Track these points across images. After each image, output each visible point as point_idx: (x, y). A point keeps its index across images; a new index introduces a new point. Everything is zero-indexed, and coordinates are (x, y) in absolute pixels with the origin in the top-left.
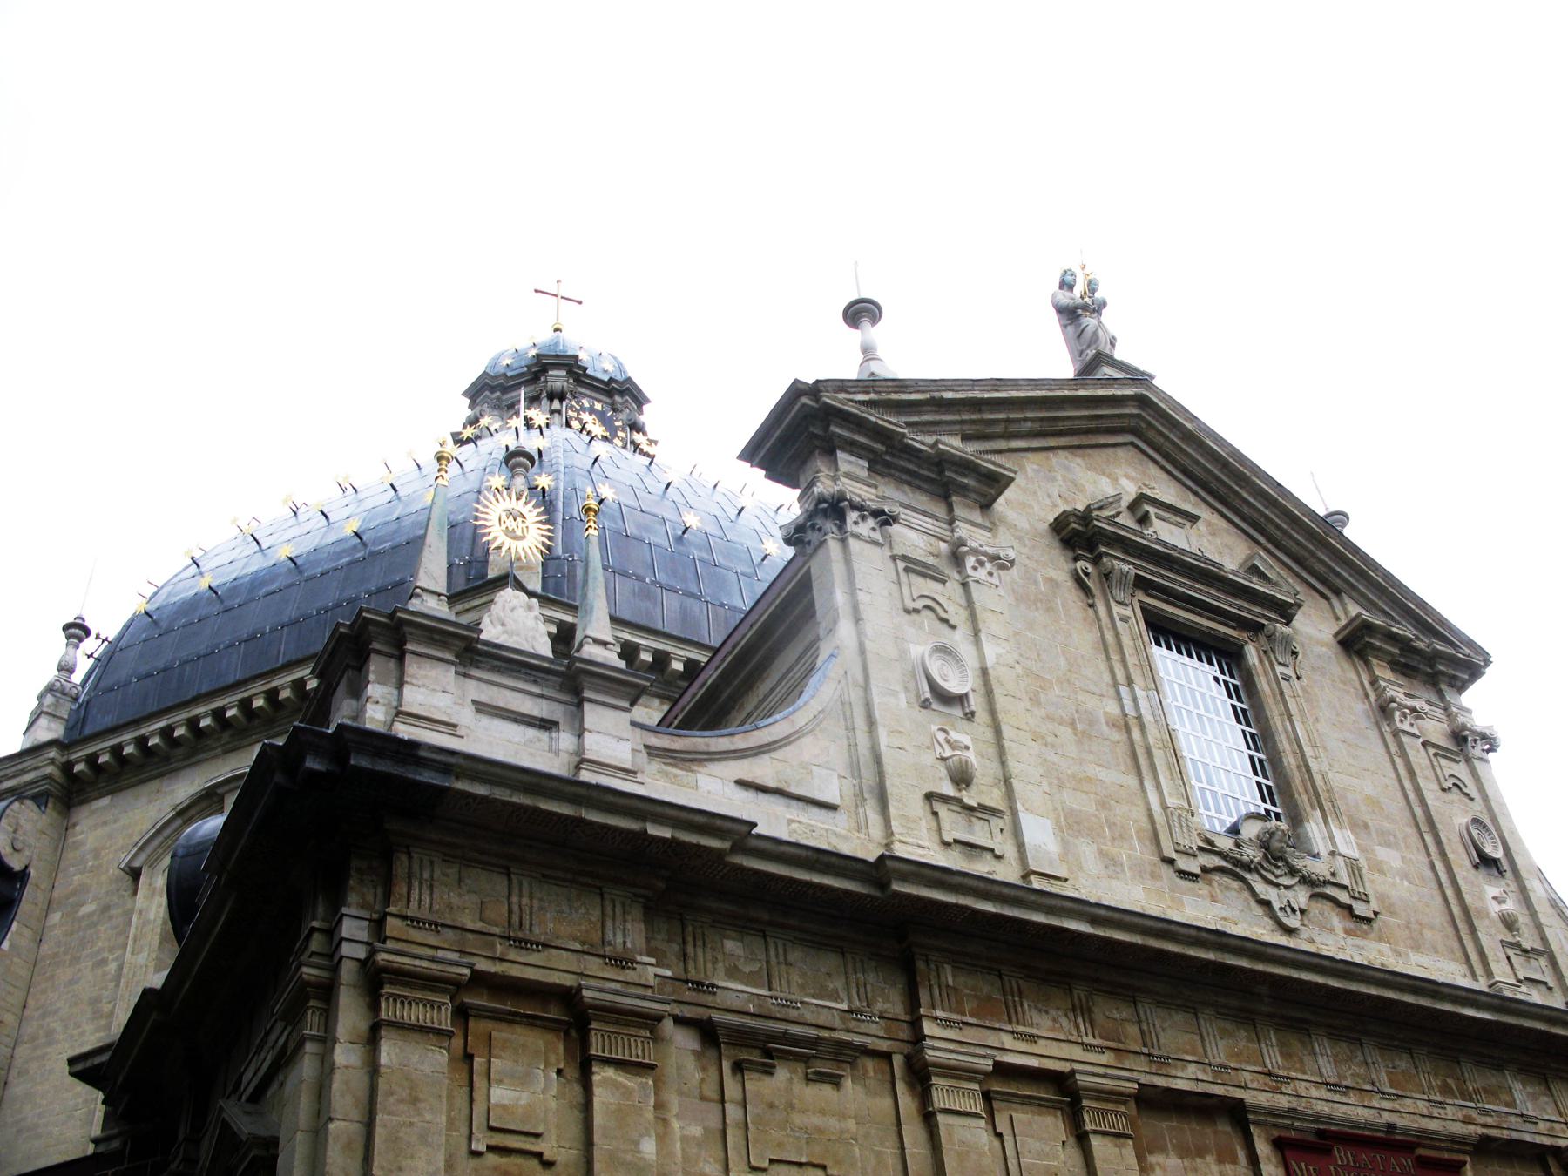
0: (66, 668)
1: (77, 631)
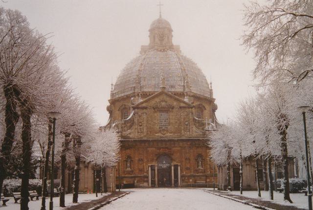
0: (112, 89)
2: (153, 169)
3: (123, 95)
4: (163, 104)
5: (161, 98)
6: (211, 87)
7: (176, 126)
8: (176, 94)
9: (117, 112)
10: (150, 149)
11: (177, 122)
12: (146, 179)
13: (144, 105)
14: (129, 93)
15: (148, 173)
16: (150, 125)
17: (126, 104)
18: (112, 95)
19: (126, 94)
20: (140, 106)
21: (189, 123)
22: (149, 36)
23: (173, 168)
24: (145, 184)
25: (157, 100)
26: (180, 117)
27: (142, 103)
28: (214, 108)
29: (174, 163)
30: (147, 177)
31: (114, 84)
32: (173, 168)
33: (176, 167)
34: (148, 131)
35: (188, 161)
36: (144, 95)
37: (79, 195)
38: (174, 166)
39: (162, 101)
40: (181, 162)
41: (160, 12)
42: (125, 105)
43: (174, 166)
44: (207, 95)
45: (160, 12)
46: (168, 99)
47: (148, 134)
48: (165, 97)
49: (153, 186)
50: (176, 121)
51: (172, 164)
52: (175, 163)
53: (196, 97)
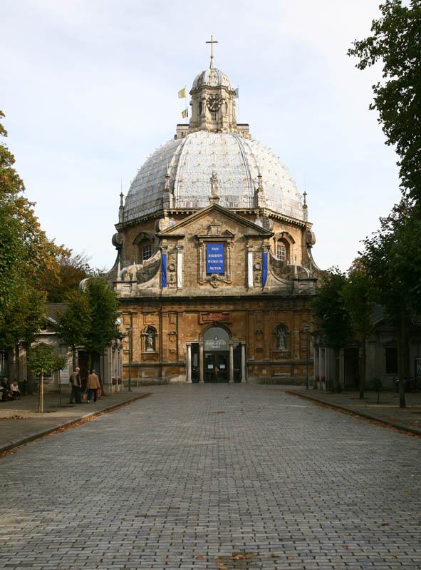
1: (122, 195)
45: (212, 58)
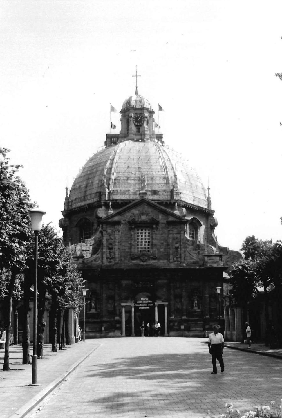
0: (67, 194)
1: (67, 189)
2: (128, 312)
3: (82, 204)
4: (144, 218)
5: (140, 208)
6: (209, 194)
7: (161, 250)
8: (160, 202)
9: (74, 229)
10: (124, 283)
11: (162, 244)
12: (118, 325)
13: (116, 219)
14: (92, 201)
15: (121, 316)
16: (123, 248)
17: (88, 217)
18: (68, 202)
19: (88, 202)
20: (110, 220)
21: (181, 245)
22: (121, 120)
23: (156, 309)
24: (118, 333)
25: (136, 212)
26: (168, 237)
27: (113, 216)
28: (212, 226)
29: (158, 303)
30: (120, 322)
31: (70, 188)
32: (156, 309)
33: (161, 308)
34: (121, 256)
35: (178, 300)
36: (116, 204)
37: (4, 357)
38: (159, 306)
39: (143, 214)
40: (168, 300)
41: (137, 87)
42: (86, 219)
43: (159, 306)
44: (204, 205)
45: (137, 87)
46: (150, 210)
47: (121, 260)
48: (146, 208)
49: (129, 334)
50: (162, 242)
51: (156, 304)
52: (160, 303)
53: (191, 209)
